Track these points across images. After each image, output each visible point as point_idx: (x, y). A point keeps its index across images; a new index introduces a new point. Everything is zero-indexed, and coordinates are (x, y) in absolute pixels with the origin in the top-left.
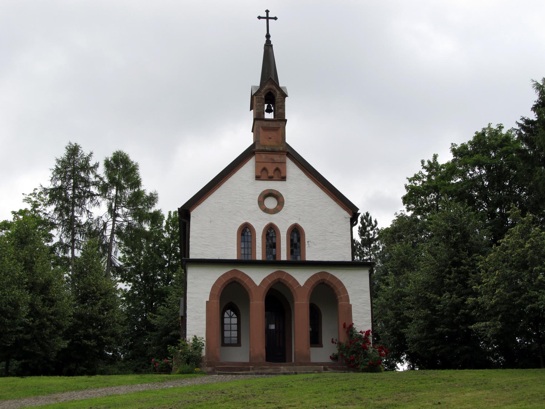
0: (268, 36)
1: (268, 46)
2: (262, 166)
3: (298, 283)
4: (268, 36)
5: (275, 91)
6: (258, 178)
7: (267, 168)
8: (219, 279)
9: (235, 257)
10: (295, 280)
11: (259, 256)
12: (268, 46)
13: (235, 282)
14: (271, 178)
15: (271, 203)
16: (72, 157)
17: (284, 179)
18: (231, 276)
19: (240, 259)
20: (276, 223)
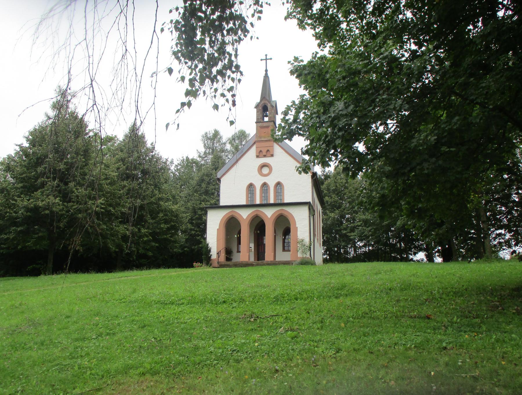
0: (266, 71)
1: (266, 78)
2: (259, 149)
3: (267, 216)
4: (266, 71)
5: (267, 104)
6: (258, 157)
7: (262, 150)
8: (225, 216)
9: (244, 203)
10: (239, 214)
11: (272, 201)
12: (266, 78)
13: (233, 217)
14: (265, 156)
15: (265, 171)
16: (415, 118)
17: (272, 155)
18: (255, 213)
19: (248, 204)
20: (267, 182)
